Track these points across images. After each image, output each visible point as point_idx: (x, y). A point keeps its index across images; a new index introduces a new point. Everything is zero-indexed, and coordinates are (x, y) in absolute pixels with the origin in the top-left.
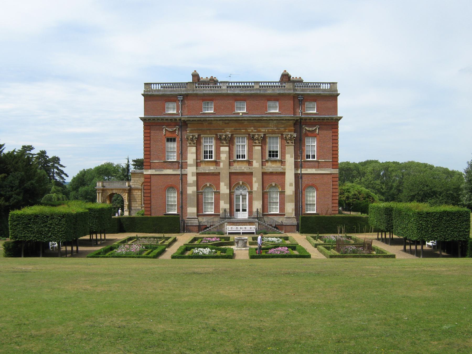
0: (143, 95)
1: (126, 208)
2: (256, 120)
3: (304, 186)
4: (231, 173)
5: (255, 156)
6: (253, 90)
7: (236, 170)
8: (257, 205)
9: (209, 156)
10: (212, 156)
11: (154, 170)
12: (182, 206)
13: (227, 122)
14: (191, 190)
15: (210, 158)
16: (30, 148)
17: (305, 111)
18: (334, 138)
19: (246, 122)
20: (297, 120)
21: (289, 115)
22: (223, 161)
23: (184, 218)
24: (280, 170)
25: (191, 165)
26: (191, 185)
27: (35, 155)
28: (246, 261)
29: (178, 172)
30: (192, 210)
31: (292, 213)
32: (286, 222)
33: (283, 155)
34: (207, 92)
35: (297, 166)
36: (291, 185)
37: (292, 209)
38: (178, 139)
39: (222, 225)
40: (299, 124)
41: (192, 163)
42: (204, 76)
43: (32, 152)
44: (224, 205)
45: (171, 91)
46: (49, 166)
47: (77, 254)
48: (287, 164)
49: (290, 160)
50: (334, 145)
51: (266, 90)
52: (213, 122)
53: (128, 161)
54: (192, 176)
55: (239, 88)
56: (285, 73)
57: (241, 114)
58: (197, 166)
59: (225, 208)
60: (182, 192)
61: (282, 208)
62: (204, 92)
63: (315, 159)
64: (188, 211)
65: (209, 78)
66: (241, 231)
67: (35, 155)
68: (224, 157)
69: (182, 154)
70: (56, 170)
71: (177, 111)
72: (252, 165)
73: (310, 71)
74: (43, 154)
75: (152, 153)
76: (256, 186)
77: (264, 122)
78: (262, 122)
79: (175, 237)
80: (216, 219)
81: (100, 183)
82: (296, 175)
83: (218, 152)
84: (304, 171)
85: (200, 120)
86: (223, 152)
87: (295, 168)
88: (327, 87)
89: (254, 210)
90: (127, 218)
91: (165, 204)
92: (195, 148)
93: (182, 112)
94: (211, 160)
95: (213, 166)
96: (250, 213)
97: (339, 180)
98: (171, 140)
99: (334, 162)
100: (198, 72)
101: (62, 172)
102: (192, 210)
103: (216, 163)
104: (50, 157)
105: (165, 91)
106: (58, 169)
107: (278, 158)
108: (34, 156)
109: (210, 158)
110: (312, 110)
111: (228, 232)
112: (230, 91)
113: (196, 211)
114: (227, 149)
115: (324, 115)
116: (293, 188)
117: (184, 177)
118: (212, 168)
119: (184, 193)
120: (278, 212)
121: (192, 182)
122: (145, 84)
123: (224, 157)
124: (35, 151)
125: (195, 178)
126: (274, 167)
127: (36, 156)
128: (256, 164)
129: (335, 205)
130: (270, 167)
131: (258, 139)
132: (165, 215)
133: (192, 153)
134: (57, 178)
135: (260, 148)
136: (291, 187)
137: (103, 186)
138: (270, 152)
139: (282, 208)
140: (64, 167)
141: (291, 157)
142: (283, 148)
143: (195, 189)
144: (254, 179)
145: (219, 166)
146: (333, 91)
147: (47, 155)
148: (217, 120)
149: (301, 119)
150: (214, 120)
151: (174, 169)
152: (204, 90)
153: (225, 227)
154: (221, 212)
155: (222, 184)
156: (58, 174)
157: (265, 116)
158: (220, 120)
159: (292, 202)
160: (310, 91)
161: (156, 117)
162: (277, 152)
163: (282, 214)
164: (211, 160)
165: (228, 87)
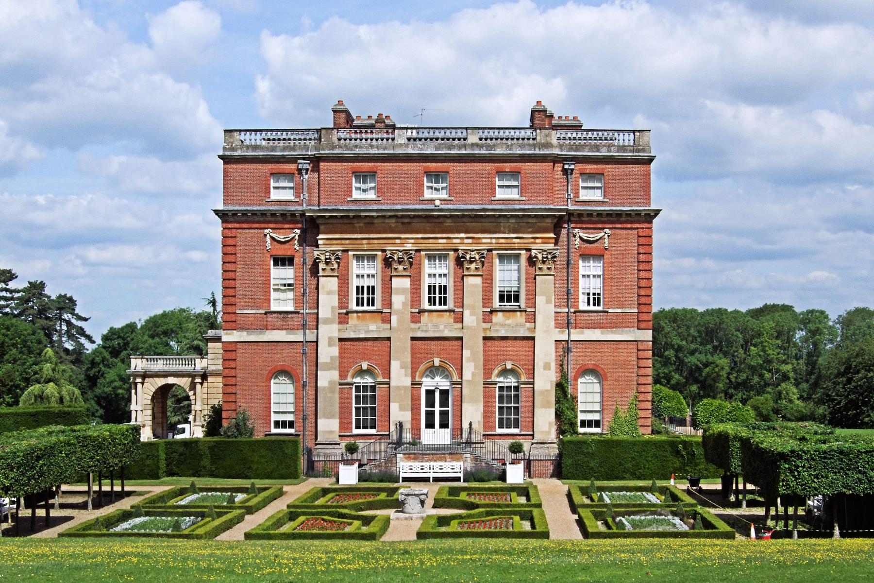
0: (220, 157)
2: (469, 216)
9: (368, 299)
11: (245, 333)
13: (406, 220)
15: (368, 305)
17: (574, 189)
19: (449, 220)
25: (327, 321)
27: (19, 291)
31: (549, 433)
36: (547, 367)
37: (550, 423)
39: (391, 460)
42: (361, 113)
45: (284, 149)
49: (546, 308)
50: (642, 274)
51: (493, 147)
52: (376, 221)
54: (330, 345)
55: (435, 143)
56: (538, 108)
57: (437, 203)
62: (357, 151)
66: (431, 475)
67: (19, 291)
68: (399, 301)
69: (309, 295)
74: (36, 288)
77: (486, 220)
78: (483, 220)
79: (279, 486)
80: (383, 446)
83: (388, 292)
85: (348, 217)
88: (627, 140)
93: (308, 195)
95: (375, 322)
97: (654, 355)
98: (283, 261)
100: (348, 106)
101: (82, 332)
105: (273, 149)
106: (69, 323)
108: (16, 295)
109: (368, 305)
111: (402, 475)
112: (413, 149)
114: (406, 283)
115: (621, 205)
118: (373, 328)
121: (328, 360)
122: (226, 131)
125: (335, 351)
127: (20, 295)
132: (266, 435)
133: (329, 293)
135: (479, 280)
136: (546, 372)
140: (86, 320)
141: (548, 302)
143: (335, 375)
144: (466, 353)
146: (638, 151)
148: (384, 216)
150: (378, 216)
151: (291, 329)
152: (356, 146)
154: (392, 428)
155: (395, 365)
156: (70, 337)
157: (490, 207)
158: (391, 217)
161: (249, 208)
164: (371, 308)
165: (409, 139)
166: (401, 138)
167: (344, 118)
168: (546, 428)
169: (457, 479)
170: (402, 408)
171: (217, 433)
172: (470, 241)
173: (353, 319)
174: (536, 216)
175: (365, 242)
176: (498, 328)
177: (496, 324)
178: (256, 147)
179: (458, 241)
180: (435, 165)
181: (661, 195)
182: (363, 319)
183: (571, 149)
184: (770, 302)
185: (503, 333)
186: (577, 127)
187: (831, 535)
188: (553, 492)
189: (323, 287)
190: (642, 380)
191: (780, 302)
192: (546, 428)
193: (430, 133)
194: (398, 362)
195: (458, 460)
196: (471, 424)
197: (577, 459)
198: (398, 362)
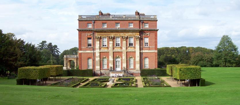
0: (78, 20)
1: (65, 65)
3: (143, 57)
4: (100, 52)
6: (123, 18)
8: (124, 65)
12: (94, 66)
14: (97, 59)
16: (45, 42)
17: (143, 27)
20: (140, 31)
21: (137, 28)
22: (110, 47)
23: (95, 71)
24: (134, 51)
25: (97, 49)
26: (97, 57)
28: (110, 88)
29: (92, 52)
30: (98, 67)
32: (136, 72)
34: (104, 19)
35: (140, 49)
36: (138, 57)
38: (92, 38)
39: (109, 74)
40: (141, 32)
41: (98, 48)
42: (104, 13)
43: (46, 43)
44: (111, 65)
45: (90, 19)
47: (46, 84)
48: (136, 48)
49: (138, 46)
51: (128, 18)
54: (98, 53)
58: (100, 49)
59: (111, 66)
60: (94, 60)
63: (148, 46)
64: (63, 68)
65: (107, 13)
70: (56, 50)
71: (92, 27)
72: (122, 49)
73: (146, 11)
74: (50, 44)
75: (82, 44)
76: (124, 57)
82: (140, 53)
84: (143, 51)
87: (140, 50)
90: (76, 70)
91: (88, 66)
92: (99, 42)
93: (93, 27)
94: (105, 47)
96: (122, 68)
99: (156, 48)
101: (58, 51)
102: (98, 67)
104: (53, 45)
105: (87, 19)
106: (57, 50)
107: (133, 46)
110: (147, 26)
111: (111, 76)
113: (99, 68)
116: (139, 58)
117: (94, 54)
118: (106, 50)
119: (95, 60)
120: (133, 68)
121: (98, 56)
122: (79, 16)
123: (111, 46)
124: (47, 43)
125: (99, 54)
128: (124, 48)
129: (156, 65)
130: (130, 50)
131: (125, 38)
133: (98, 44)
134: (56, 53)
137: (66, 57)
138: (130, 44)
141: (138, 45)
142: (135, 42)
143: (99, 58)
144: (123, 55)
149: (142, 30)
151: (90, 50)
156: (57, 52)
159: (139, 64)
160: (146, 18)
162: (132, 44)
163: (134, 69)
164: (119, 46)
166: (111, 17)
167: (101, 14)
168: (138, 68)
169: (122, 77)
170: (111, 64)
171: (179, 80)
173: (102, 49)
174: (136, 30)
178: (85, 19)
182: (104, 49)
183: (147, 19)
184: (183, 46)
186: (144, 15)
187: (196, 86)
188: (139, 78)
190: (156, 62)
191: (184, 46)
192: (138, 68)
193: (114, 16)
195: (121, 73)
196: (124, 67)
197: (144, 73)
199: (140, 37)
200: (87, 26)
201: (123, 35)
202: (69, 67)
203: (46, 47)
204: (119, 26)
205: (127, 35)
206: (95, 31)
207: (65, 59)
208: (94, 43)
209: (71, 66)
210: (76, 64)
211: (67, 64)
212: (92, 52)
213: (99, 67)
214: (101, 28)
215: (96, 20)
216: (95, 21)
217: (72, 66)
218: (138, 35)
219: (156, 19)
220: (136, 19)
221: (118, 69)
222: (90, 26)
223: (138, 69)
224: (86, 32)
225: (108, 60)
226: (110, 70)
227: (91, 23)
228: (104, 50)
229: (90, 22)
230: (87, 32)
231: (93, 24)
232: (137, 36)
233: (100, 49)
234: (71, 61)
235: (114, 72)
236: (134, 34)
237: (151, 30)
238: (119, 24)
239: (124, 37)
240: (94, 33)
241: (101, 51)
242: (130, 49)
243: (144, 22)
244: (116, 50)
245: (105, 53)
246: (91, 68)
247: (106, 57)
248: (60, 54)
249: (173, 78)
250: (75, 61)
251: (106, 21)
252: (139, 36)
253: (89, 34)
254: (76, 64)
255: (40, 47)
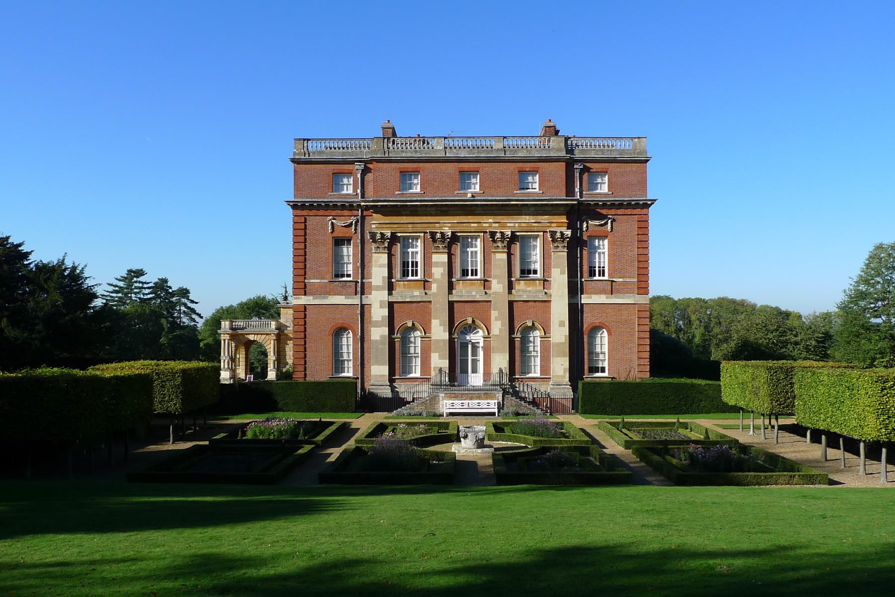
5: (494, 272)
7: (461, 296)
8: (500, 361)
9: (412, 271)
10: (417, 271)
11: (311, 297)
13: (445, 209)
14: (378, 333)
16: (140, 273)
18: (642, 238)
21: (558, 195)
22: (436, 281)
25: (378, 288)
26: (378, 324)
29: (356, 300)
31: (564, 376)
33: (546, 267)
36: (562, 324)
37: (565, 369)
39: (433, 399)
43: (142, 279)
45: (344, 154)
46: (172, 302)
49: (559, 279)
50: (641, 251)
53: (286, 292)
54: (381, 307)
61: (545, 369)
63: (606, 277)
70: (183, 308)
71: (355, 190)
72: (490, 288)
76: (499, 326)
81: (227, 323)
86: (438, 264)
89: (495, 370)
91: (338, 364)
94: (414, 278)
95: (419, 289)
96: (487, 374)
102: (379, 371)
103: (425, 284)
104: (175, 288)
106: (185, 305)
111: (446, 411)
116: (566, 330)
117: (363, 309)
120: (538, 375)
123: (439, 272)
124: (151, 278)
125: (385, 312)
126: (530, 291)
128: (498, 286)
129: (642, 362)
133: (381, 266)
137: (232, 328)
139: (545, 369)
143: (385, 331)
144: (494, 314)
145: (430, 289)
147: (169, 284)
149: (580, 203)
151: (347, 295)
153: (441, 402)
154: (433, 373)
163: (545, 378)
168: (561, 373)
170: (441, 357)
172: (497, 225)
175: (410, 226)
176: (521, 293)
177: (519, 290)
179: (487, 225)
180: (466, 166)
181: (656, 186)
185: (525, 298)
189: (376, 261)
190: (641, 348)
192: (561, 373)
194: (438, 321)
195: (492, 398)
198: (438, 321)
199: (569, 233)
200: (336, 185)
201: (495, 227)
202: (241, 373)
203: (144, 294)
204: (478, 186)
205: (511, 224)
206: (367, 208)
207: (227, 337)
208: (366, 261)
209: (250, 369)
210: (271, 358)
211: (233, 360)
212: (356, 300)
213: (384, 370)
214: (396, 196)
215: (371, 161)
216: (366, 162)
217: (257, 367)
218: (560, 224)
219: (640, 153)
220: (552, 154)
221: (476, 380)
222: (348, 188)
223: (559, 380)
224: (326, 213)
225: (426, 338)
226: (432, 381)
227: (349, 174)
228: (405, 293)
229: (346, 167)
230: (334, 213)
231: (359, 176)
232: (558, 230)
233: (391, 288)
234: (253, 348)
235: (456, 390)
236: (545, 219)
237: (620, 205)
238: (475, 177)
239: (498, 235)
240: (363, 218)
241: (397, 297)
242: (524, 290)
243: (588, 165)
244: (462, 292)
245: (415, 305)
246: (351, 374)
247: (417, 324)
248: (200, 323)
249: (773, 427)
250: (270, 348)
251: (415, 165)
252: (564, 230)
253: (339, 223)
254: (271, 358)
255: (120, 295)
